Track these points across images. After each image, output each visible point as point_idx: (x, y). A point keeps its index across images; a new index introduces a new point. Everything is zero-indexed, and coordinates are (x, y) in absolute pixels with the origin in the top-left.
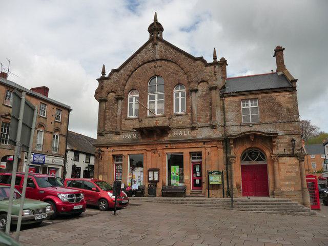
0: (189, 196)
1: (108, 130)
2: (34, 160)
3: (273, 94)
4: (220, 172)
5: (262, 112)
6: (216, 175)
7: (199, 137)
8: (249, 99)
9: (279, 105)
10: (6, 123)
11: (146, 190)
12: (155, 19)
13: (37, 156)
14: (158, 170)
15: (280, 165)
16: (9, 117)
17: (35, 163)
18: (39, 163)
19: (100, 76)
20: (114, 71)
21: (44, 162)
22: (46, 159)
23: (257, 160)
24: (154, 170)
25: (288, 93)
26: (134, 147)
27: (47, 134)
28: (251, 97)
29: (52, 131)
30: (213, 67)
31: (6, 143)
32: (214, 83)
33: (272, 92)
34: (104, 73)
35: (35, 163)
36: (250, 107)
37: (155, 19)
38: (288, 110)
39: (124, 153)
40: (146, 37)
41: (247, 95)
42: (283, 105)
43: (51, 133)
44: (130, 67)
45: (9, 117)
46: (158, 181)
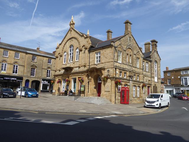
16: (34, 66)
26: (64, 76)
31: (34, 76)
45: (34, 66)
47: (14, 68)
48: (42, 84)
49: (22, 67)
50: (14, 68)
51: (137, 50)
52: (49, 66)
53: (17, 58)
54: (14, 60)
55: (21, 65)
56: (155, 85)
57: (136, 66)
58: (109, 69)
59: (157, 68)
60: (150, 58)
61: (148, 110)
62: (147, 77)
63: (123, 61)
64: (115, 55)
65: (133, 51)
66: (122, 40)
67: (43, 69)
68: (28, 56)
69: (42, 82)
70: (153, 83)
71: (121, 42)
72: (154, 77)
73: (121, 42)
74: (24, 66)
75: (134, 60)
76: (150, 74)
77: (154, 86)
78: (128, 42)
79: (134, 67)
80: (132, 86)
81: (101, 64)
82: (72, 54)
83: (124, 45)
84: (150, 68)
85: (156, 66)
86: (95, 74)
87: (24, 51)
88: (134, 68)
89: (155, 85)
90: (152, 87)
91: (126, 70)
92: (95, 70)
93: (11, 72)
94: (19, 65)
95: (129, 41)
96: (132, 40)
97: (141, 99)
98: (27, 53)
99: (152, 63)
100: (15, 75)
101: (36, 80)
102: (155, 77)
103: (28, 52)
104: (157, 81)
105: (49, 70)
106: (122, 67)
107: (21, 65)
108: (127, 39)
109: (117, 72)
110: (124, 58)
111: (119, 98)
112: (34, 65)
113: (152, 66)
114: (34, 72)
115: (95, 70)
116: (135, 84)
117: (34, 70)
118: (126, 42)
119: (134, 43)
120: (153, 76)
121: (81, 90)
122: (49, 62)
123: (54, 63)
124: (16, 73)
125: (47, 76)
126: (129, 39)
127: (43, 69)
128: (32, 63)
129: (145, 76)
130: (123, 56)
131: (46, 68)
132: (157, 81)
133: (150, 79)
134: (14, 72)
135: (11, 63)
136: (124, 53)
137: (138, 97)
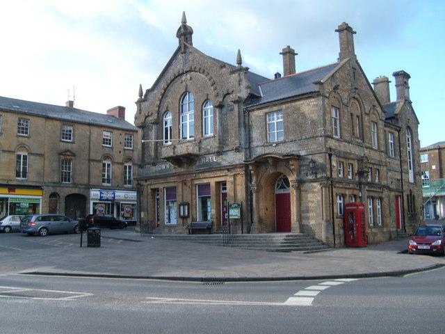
0: (215, 233)
1: (315, 184)
2: (101, 197)
3: (298, 103)
4: (239, 205)
5: (286, 128)
6: (235, 207)
7: (224, 163)
8: (273, 112)
9: (303, 115)
10: (66, 160)
11: (215, 227)
12: (184, 22)
13: (105, 192)
14: (188, 204)
15: (302, 193)
16: (68, 153)
17: (104, 200)
18: (107, 200)
19: (137, 98)
20: (148, 91)
21: (114, 198)
22: (116, 194)
23: (280, 188)
24: (183, 204)
25: (313, 100)
26: (168, 179)
27: (116, 166)
28: (275, 108)
29: (121, 161)
30: (237, 74)
31: (69, 181)
32: (239, 95)
33: (295, 101)
34: (141, 94)
35: (104, 200)
36: (153, 140)
37: (184, 22)
38: (313, 121)
39: (161, 187)
40: (175, 43)
41: (271, 106)
42: (308, 116)
43: (122, 164)
44: (163, 85)
45: (68, 153)
46: (188, 216)
47: (18, 162)
49: (38, 157)
50: (18, 162)
52: (107, 151)
53: (108, 146)
54: (18, 141)
55: (37, 154)
56: (410, 191)
59: (413, 148)
61: (253, 285)
62: (394, 173)
64: (327, 118)
65: (362, 105)
66: (337, 78)
67: (93, 160)
68: (50, 124)
74: (41, 155)
76: (399, 163)
79: (367, 148)
80: (366, 198)
84: (398, 148)
85: (338, 122)
86: (271, 171)
88: (367, 151)
89: (410, 191)
90: (405, 198)
91: (352, 156)
92: (270, 161)
93: (13, 174)
94: (31, 154)
97: (385, 230)
99: (401, 133)
100: (22, 181)
101: (77, 192)
103: (51, 115)
105: (107, 162)
106: (342, 149)
107: (37, 154)
109: (334, 164)
111: (342, 231)
113: (402, 142)
114: (69, 170)
115: (270, 161)
116: (373, 194)
117: (69, 164)
121: (230, 217)
122: (23, 130)
123: (118, 142)
124: (24, 176)
128: (63, 146)
134: (18, 175)
135: (9, 149)
137: (380, 227)
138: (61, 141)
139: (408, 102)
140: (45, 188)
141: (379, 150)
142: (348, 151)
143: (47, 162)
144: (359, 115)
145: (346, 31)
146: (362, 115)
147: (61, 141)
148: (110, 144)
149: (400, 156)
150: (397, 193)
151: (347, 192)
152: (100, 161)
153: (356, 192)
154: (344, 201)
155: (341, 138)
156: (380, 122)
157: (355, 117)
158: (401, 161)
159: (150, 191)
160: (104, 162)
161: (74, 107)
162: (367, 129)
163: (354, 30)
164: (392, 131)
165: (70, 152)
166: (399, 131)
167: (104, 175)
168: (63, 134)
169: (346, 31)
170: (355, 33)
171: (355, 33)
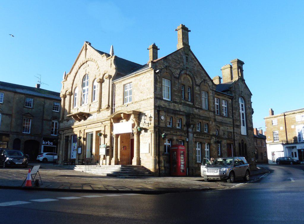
16: (29, 115)
31: (28, 132)
45: (29, 115)
48: (43, 146)
51: (201, 78)
57: (201, 106)
58: (184, 135)
60: (231, 92)
63: (174, 97)
64: (157, 86)
65: (193, 79)
66: (170, 60)
67: (45, 120)
68: (17, 97)
69: (44, 143)
70: (238, 138)
71: (169, 63)
72: (239, 127)
73: (169, 63)
75: (197, 96)
77: (239, 144)
78: (183, 62)
81: (133, 105)
82: (87, 91)
83: (175, 68)
87: (11, 89)
88: (196, 111)
92: (122, 115)
95: (185, 61)
96: (192, 60)
98: (16, 92)
102: (242, 126)
104: (246, 134)
106: (172, 108)
108: (181, 58)
110: (175, 91)
112: (28, 113)
118: (179, 64)
119: (195, 64)
120: (238, 123)
125: (52, 133)
126: (184, 57)
127: (45, 120)
129: (221, 123)
130: (174, 89)
131: (49, 119)
132: (246, 134)
133: (232, 130)
136: (174, 82)
138: (24, 107)
139: (241, 79)
140: (11, 135)
141: (209, 110)
142: (178, 109)
143: (14, 120)
144: (191, 86)
145: (185, 30)
146: (193, 87)
147: (24, 107)
148: (58, 110)
149: (233, 116)
150: (229, 142)
151: (175, 138)
152: (50, 120)
153: (183, 138)
154: (171, 144)
155: (171, 100)
156: (211, 91)
157: (187, 88)
158: (233, 119)
159: (65, 137)
160: (53, 121)
161: (40, 88)
162: (197, 96)
163: (189, 29)
164: (226, 99)
165: (30, 114)
166: (232, 99)
167: (53, 129)
168: (54, 107)
169: (185, 30)
170: (190, 31)
171: (190, 31)
